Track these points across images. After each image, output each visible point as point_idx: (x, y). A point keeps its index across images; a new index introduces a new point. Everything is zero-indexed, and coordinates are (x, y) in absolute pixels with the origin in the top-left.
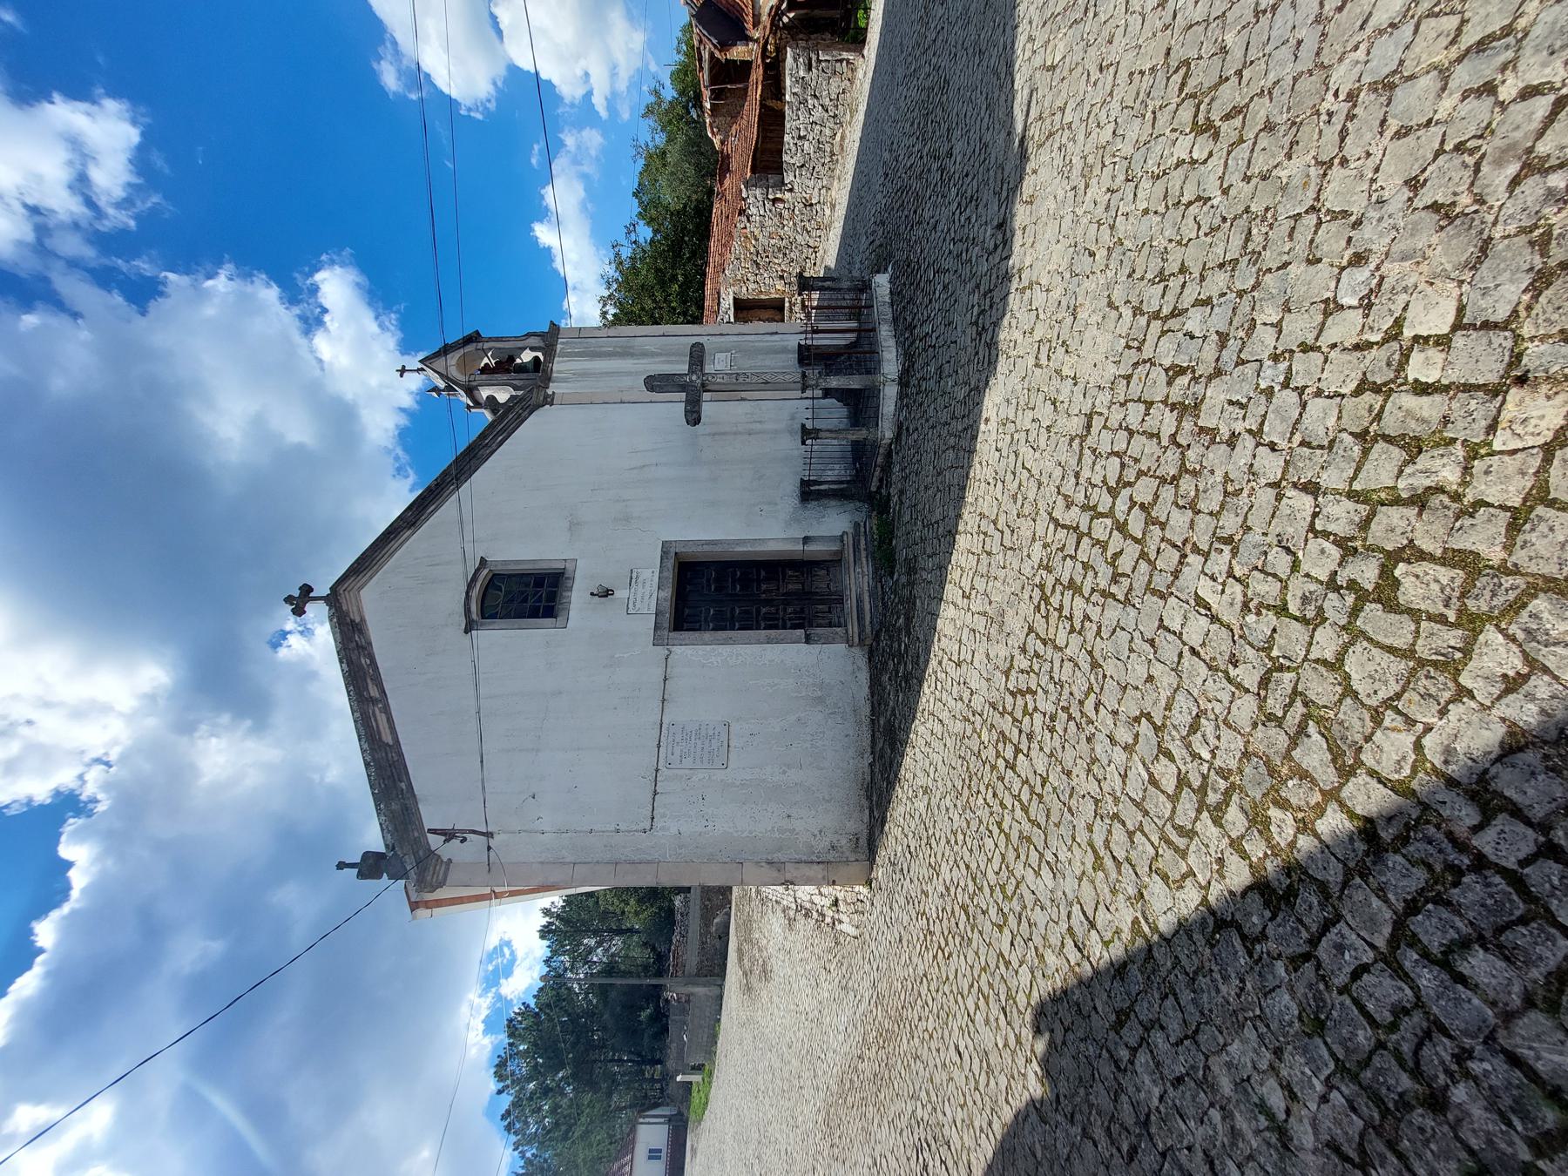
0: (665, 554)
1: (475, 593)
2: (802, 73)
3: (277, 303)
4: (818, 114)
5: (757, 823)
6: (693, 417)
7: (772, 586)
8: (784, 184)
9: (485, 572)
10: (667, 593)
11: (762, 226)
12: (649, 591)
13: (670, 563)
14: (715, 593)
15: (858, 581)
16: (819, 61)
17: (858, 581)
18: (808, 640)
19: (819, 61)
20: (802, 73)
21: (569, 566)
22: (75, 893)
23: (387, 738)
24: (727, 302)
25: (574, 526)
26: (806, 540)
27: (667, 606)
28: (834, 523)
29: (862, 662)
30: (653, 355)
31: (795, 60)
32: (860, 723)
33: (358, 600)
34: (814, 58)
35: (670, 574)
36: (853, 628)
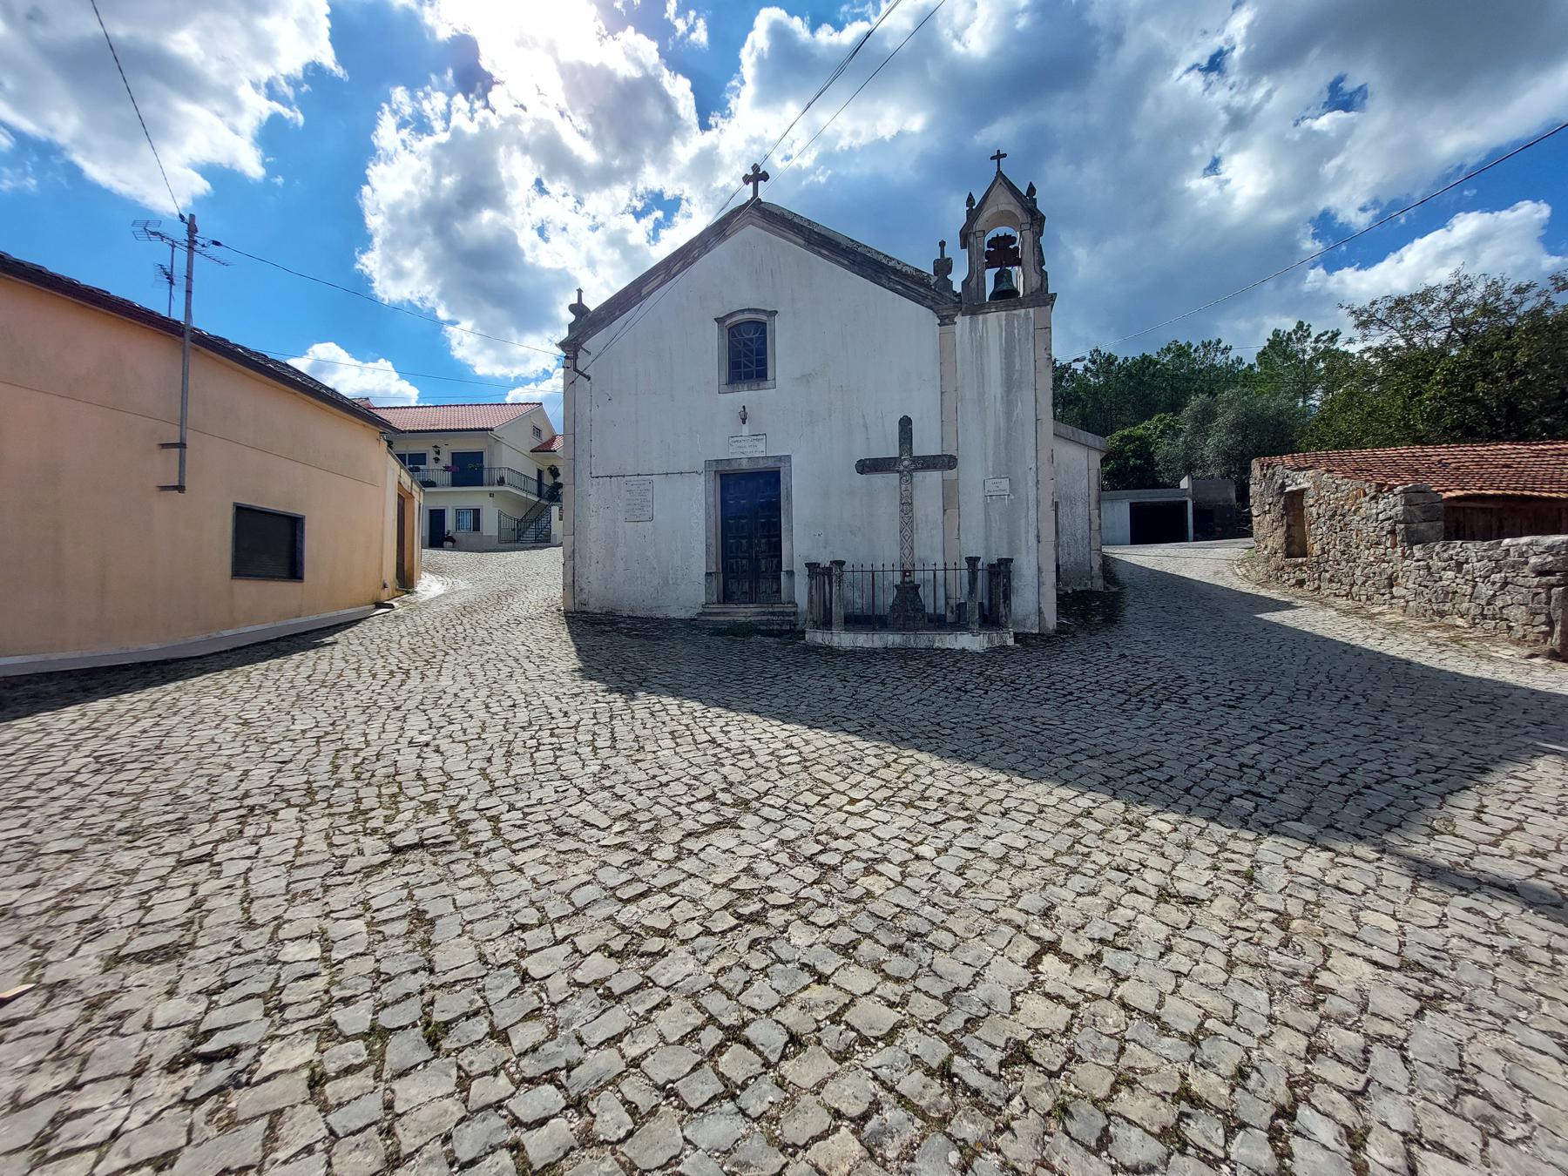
0: (779, 458)
1: (747, 316)
2: (1533, 560)
3: (376, 276)
4: (1485, 590)
5: (593, 546)
6: (868, 466)
7: (763, 548)
8: (1412, 544)
9: (764, 318)
10: (745, 465)
11: (1367, 518)
12: (747, 451)
13: (771, 464)
14: (750, 507)
15: (744, 613)
16: (1551, 586)
17: (744, 613)
18: (708, 574)
19: (1551, 586)
20: (1533, 560)
21: (769, 383)
22: (1011, 208)
23: (644, 292)
24: (1303, 481)
25: (806, 379)
26: (791, 573)
27: (735, 466)
28: (800, 591)
29: (691, 614)
30: (1009, 414)
31: (1550, 549)
32: (651, 609)
33: (742, 227)
34: (1553, 579)
35: (761, 465)
36: (715, 608)
